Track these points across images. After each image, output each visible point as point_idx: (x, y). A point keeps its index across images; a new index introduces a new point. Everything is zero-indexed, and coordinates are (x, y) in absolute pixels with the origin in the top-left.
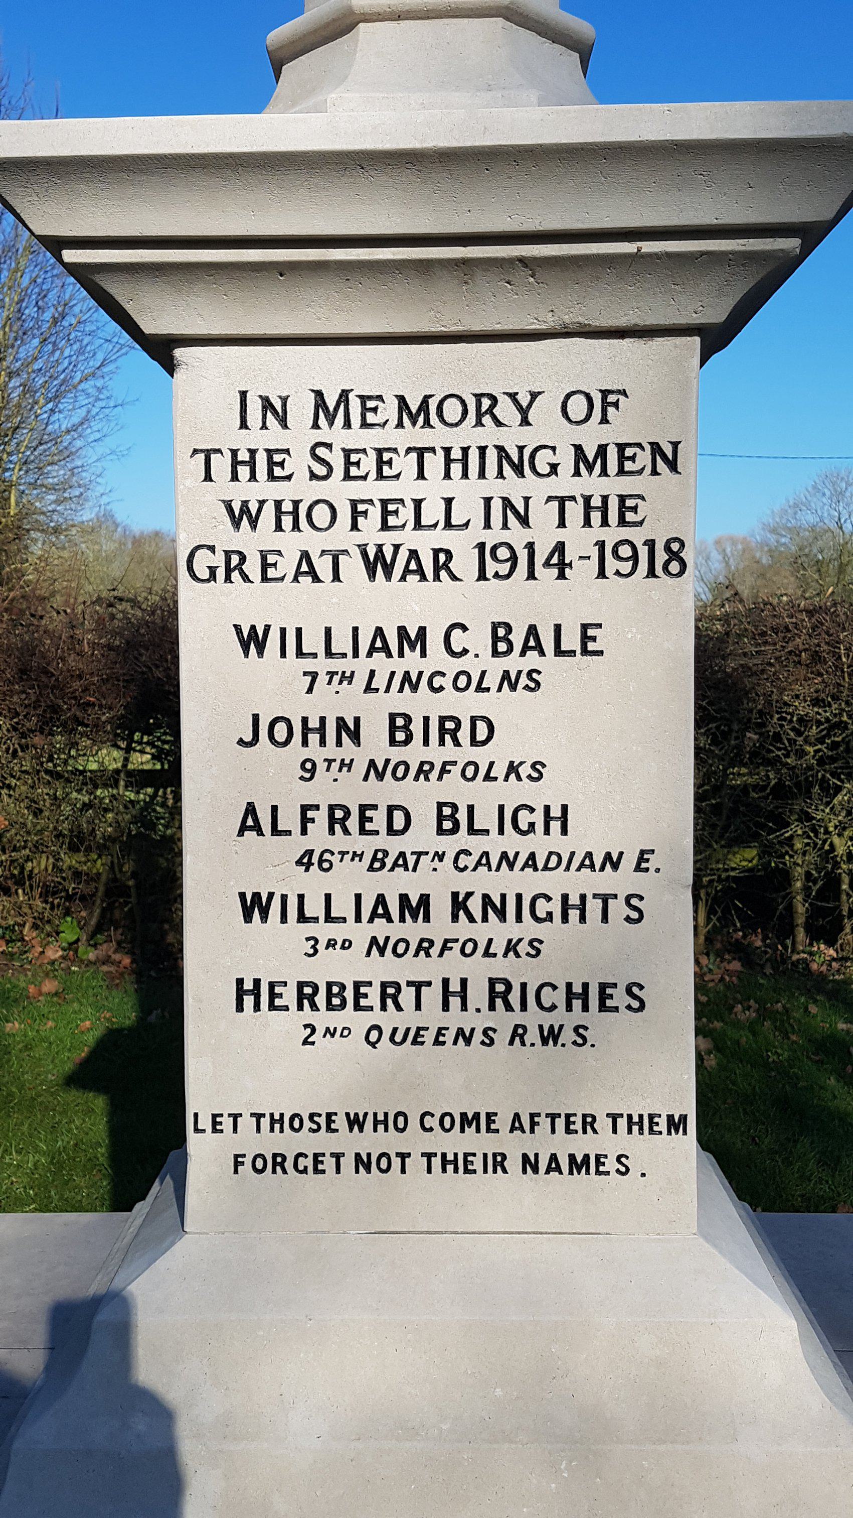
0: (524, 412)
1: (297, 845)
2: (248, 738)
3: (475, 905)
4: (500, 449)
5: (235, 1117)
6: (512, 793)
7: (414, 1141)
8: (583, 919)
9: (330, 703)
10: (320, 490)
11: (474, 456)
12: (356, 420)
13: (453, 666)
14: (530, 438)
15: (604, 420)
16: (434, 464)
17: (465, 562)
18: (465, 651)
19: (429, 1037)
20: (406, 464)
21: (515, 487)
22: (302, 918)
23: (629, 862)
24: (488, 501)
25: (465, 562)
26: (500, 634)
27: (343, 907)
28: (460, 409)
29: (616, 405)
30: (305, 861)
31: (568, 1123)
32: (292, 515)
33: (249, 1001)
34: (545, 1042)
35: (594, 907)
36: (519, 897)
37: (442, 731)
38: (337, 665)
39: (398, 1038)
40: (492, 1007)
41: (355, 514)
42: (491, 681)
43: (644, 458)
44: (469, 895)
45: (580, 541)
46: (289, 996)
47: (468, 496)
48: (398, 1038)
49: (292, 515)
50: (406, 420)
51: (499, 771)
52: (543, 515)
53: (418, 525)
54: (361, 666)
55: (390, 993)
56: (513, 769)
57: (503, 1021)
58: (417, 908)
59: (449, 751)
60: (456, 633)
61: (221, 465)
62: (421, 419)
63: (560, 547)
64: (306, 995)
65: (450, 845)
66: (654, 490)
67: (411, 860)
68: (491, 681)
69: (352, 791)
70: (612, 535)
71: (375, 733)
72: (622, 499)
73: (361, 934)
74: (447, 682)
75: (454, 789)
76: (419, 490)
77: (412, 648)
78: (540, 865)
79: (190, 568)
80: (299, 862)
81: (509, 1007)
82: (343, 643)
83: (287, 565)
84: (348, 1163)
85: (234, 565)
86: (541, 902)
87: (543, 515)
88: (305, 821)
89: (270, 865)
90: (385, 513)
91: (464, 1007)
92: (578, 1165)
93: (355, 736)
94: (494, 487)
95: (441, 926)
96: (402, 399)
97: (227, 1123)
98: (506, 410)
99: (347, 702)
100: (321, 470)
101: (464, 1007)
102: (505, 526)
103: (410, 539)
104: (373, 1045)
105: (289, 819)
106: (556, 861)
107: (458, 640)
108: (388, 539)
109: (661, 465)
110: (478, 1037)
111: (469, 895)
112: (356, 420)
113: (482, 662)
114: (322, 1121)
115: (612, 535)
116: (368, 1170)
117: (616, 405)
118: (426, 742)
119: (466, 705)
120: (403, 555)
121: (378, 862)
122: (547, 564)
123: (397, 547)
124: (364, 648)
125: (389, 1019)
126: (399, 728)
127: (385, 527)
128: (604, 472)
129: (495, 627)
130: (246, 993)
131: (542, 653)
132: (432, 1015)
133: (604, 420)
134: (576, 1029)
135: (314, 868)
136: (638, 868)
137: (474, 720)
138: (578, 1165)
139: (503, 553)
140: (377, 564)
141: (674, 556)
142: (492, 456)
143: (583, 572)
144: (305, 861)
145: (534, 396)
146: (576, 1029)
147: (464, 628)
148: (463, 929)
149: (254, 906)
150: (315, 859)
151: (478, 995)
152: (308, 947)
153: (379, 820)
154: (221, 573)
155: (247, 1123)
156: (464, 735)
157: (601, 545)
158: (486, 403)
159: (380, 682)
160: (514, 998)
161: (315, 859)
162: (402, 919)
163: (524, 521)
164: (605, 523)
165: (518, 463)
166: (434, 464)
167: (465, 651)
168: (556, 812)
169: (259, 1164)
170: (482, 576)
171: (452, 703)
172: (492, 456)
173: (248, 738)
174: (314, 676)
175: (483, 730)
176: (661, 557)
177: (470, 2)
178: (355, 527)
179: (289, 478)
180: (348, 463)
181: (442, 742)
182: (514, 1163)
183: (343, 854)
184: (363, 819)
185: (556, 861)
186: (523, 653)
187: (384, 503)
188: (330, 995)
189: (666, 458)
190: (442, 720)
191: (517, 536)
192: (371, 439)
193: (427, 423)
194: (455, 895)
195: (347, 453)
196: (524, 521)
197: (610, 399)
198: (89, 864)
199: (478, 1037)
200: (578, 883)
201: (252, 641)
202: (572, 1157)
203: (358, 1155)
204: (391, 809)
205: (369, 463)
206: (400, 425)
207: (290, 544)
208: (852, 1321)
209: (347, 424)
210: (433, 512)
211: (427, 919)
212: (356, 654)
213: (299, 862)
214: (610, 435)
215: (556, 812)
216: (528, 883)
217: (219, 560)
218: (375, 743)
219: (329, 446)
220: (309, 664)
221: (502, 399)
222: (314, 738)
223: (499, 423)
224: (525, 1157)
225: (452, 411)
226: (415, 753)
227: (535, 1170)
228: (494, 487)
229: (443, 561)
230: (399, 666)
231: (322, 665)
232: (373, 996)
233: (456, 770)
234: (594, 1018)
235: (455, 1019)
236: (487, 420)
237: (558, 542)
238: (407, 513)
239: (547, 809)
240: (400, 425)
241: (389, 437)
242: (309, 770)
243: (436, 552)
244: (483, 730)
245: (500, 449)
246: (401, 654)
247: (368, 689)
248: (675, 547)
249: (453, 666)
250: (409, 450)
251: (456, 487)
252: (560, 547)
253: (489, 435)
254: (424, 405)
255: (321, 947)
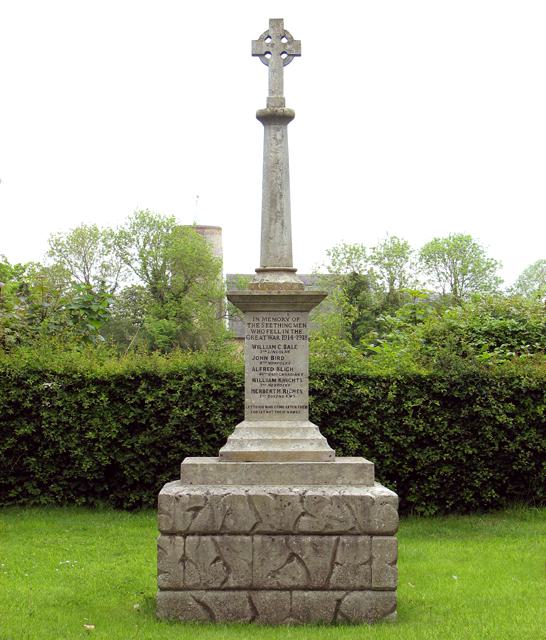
17: (281, 338)
25: (281, 338)
32: (259, 331)
47: (281, 330)
49: (259, 331)
55: (271, 391)
66: (304, 329)
71: (269, 358)
89: (256, 375)
119: (280, 355)
126: (272, 358)
130: (254, 391)
140: (270, 337)
149: (254, 380)
171: (278, 354)
175: (283, 358)
189: (305, 325)
208: (543, 609)
218: (269, 360)
226: (275, 361)
237: (298, 45)
244: (283, 358)
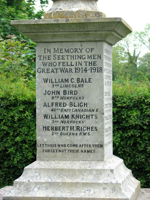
0: (81, 51)
1: (51, 108)
2: (45, 94)
3: (75, 116)
4: (78, 56)
5: (43, 145)
6: (80, 101)
7: (67, 148)
8: (89, 118)
9: (56, 89)
10: (54, 61)
11: (75, 56)
12: (59, 52)
13: (72, 84)
14: (82, 54)
15: (91, 52)
16: (69, 57)
17: (74, 71)
18: (73, 82)
19: (69, 134)
20: (66, 58)
21: (80, 61)
22: (52, 118)
23: (95, 110)
24: (76, 62)
26: (78, 80)
27: (57, 117)
28: (71, 51)
29: (93, 50)
30: (52, 110)
31: (87, 146)
32: (51, 64)
33: (45, 129)
34: (84, 135)
35: (91, 117)
36: (81, 115)
37: (70, 92)
38: (56, 84)
39: (65, 134)
40: (77, 130)
41: (59, 64)
42: (77, 86)
43: (96, 57)
44: (74, 115)
45: (88, 67)
46: (50, 129)
48: (65, 134)
49: (51, 64)
50: (66, 52)
51: (78, 98)
52: (84, 64)
53: (67, 65)
54: (60, 84)
55: (63, 128)
56: (80, 98)
57: (78, 132)
58: (67, 117)
59: (71, 96)
60: (72, 80)
61: (42, 58)
62: (91, 58)
63: (86, 68)
64: (52, 129)
65: (71, 108)
67: (66, 110)
68: (77, 86)
69: (59, 101)
70: (93, 67)
72: (94, 62)
73: (60, 120)
74: (71, 86)
75: (72, 100)
76: (67, 61)
77: (67, 82)
78: (84, 111)
79: (38, 71)
80: (51, 110)
81: (79, 130)
82: (57, 81)
83: (50, 70)
84: (58, 151)
85: (43, 71)
86: (84, 116)
87: (84, 64)
88: (52, 105)
90: (63, 64)
91: (73, 130)
92: (88, 151)
93: (59, 93)
94: (77, 60)
95: (70, 119)
96: (65, 49)
97: (42, 145)
98: (79, 51)
99: (58, 89)
100: (55, 58)
101: (73, 130)
102: (79, 66)
103: (66, 67)
104: (61, 135)
105: (50, 105)
106: (85, 110)
107: (73, 80)
108: (64, 67)
109: (99, 58)
110: (75, 134)
111: (74, 115)
112: (59, 52)
113: (75, 83)
114: (54, 145)
115: (93, 67)
116: (61, 152)
117: (93, 50)
118: (68, 94)
119: (73, 89)
120: (65, 69)
121: (62, 110)
122: (84, 70)
123: (64, 68)
124: (60, 81)
125: (63, 132)
126: (65, 92)
127: (63, 66)
128: (91, 59)
129: (77, 79)
130: (46, 128)
131: (84, 82)
132: (69, 131)
133: (91, 52)
134: (88, 133)
135: (53, 111)
136: (96, 111)
137: (75, 91)
138: (88, 151)
139: (78, 69)
141: (101, 69)
142: (77, 56)
143: (89, 72)
144: (52, 110)
145: (82, 49)
146: (88, 133)
147: (73, 79)
148: (74, 120)
149: (46, 116)
150: (54, 110)
151: (75, 128)
152: (53, 122)
153: (62, 105)
154: (42, 72)
155: (45, 146)
156: (73, 93)
157: (91, 68)
158: (76, 50)
159: (62, 86)
160: (80, 129)
161: (54, 110)
162: (65, 118)
163: (81, 65)
164: (92, 65)
165: (81, 57)
166: (69, 57)
167: (73, 82)
168: (86, 104)
169: (46, 151)
170: (76, 72)
172: (77, 56)
173: (45, 94)
174: (53, 85)
175: (76, 93)
176: (99, 70)
177: (129, 26)
178: (59, 66)
179: (50, 59)
180: (58, 57)
181: (70, 94)
182: (80, 151)
183: (57, 109)
184: (60, 105)
185: (85, 110)
186: (81, 82)
187: (63, 62)
188: (55, 128)
190: (70, 91)
191: (80, 67)
192: (61, 54)
193: (69, 52)
194: (72, 115)
195: (58, 56)
196: (81, 65)
197: (92, 49)
198: (144, 112)
199: (75, 134)
200: (88, 113)
201: (46, 81)
202: (88, 150)
203: (59, 150)
204: (64, 103)
205: (61, 57)
206: (65, 52)
207: (51, 68)
209: (58, 53)
210: (69, 64)
211: (68, 118)
212: (59, 82)
213: (51, 110)
214: (92, 54)
215: (86, 104)
216: (82, 114)
217: (41, 70)
218: (62, 94)
219: (56, 55)
220: (53, 84)
221: (78, 49)
222: (53, 94)
223: (78, 52)
224: (81, 150)
225: (72, 51)
226: (67, 96)
227: (83, 152)
228: (77, 60)
229: (71, 70)
230: (65, 84)
231: (55, 84)
232: (61, 128)
233: (72, 98)
234: (91, 132)
235: (72, 132)
236: (76, 52)
238: (66, 64)
239: (84, 103)
240: (65, 52)
241: (64, 54)
242: (53, 98)
243: (70, 69)
244: (76, 93)
245: (78, 56)
246: (65, 82)
247: (61, 87)
248: (101, 68)
249: (72, 84)
250: (66, 56)
251: (72, 60)
252: (86, 68)
253: (77, 54)
254: (68, 50)
255: (54, 122)
